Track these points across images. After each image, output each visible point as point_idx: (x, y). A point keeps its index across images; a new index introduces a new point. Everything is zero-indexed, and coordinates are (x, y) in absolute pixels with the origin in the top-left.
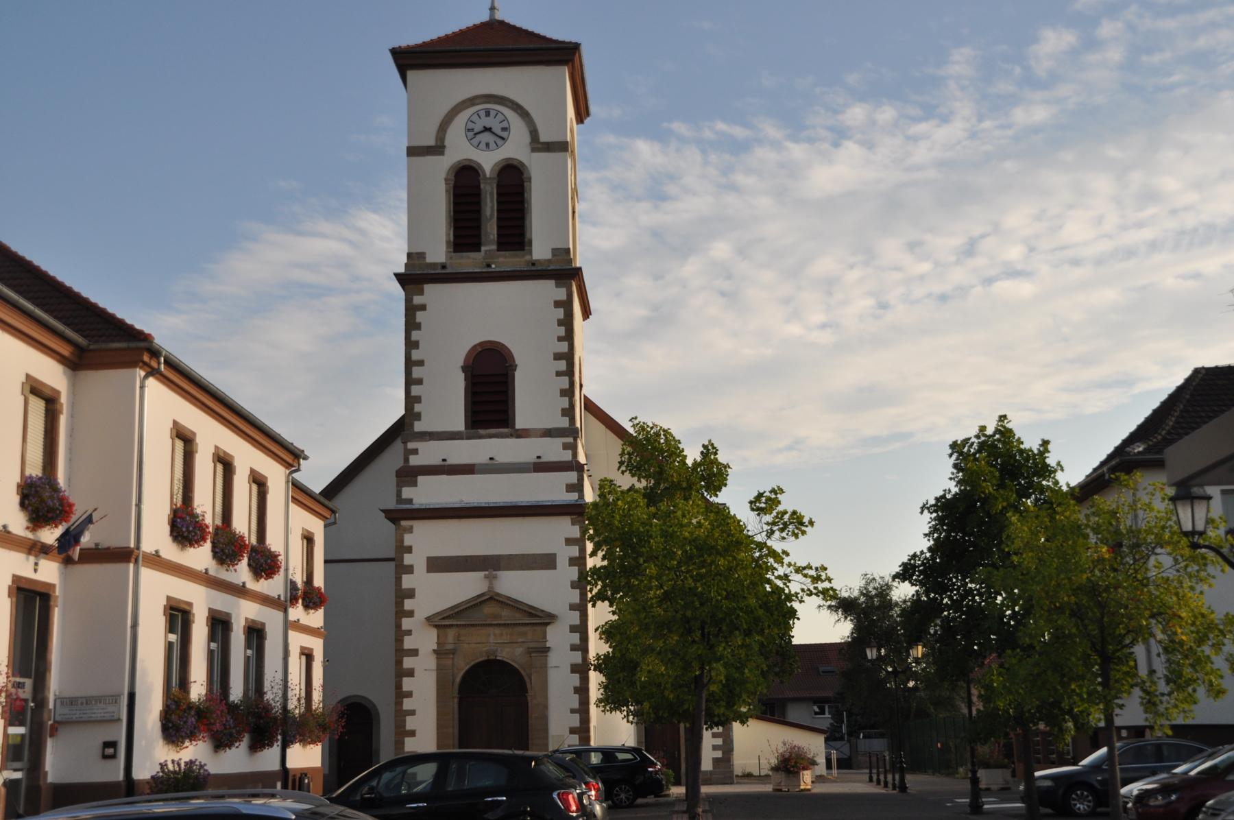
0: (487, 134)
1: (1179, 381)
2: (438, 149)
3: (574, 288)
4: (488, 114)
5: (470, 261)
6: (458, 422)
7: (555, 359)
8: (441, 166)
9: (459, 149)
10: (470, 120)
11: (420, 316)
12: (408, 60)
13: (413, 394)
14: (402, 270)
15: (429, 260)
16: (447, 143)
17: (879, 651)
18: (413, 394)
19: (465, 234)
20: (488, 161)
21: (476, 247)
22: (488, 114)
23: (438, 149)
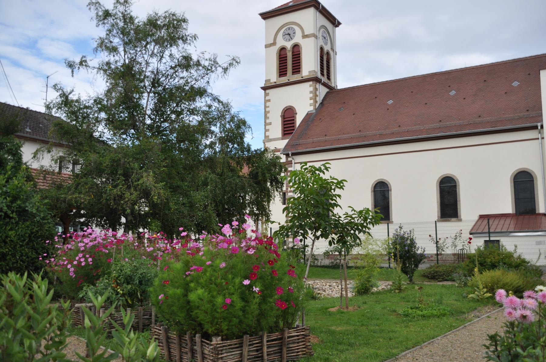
0: (288, 36)
1: (12, 104)
2: (274, 44)
3: (276, 349)
4: (289, 29)
5: (284, 80)
6: (280, 135)
7: (339, 24)
8: (274, 50)
9: (281, 42)
10: (284, 32)
11: (268, 115)
12: (266, 16)
13: (267, 135)
14: (263, 86)
15: (272, 81)
16: (277, 41)
17: (88, 258)
18: (267, 135)
19: (282, 72)
20: (289, 45)
21: (285, 75)
22: (289, 29)
23: (274, 44)
